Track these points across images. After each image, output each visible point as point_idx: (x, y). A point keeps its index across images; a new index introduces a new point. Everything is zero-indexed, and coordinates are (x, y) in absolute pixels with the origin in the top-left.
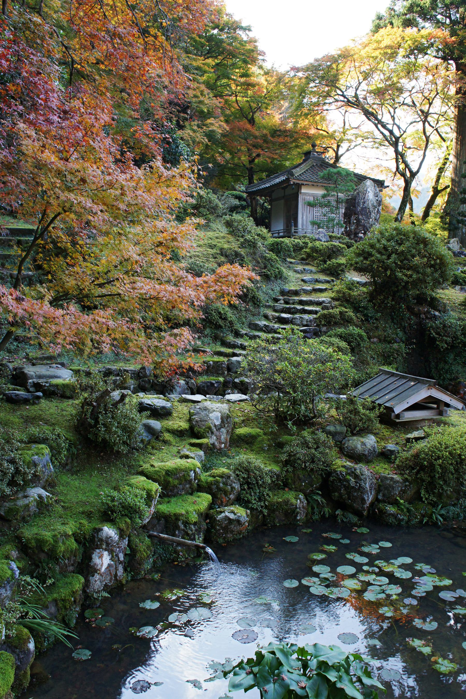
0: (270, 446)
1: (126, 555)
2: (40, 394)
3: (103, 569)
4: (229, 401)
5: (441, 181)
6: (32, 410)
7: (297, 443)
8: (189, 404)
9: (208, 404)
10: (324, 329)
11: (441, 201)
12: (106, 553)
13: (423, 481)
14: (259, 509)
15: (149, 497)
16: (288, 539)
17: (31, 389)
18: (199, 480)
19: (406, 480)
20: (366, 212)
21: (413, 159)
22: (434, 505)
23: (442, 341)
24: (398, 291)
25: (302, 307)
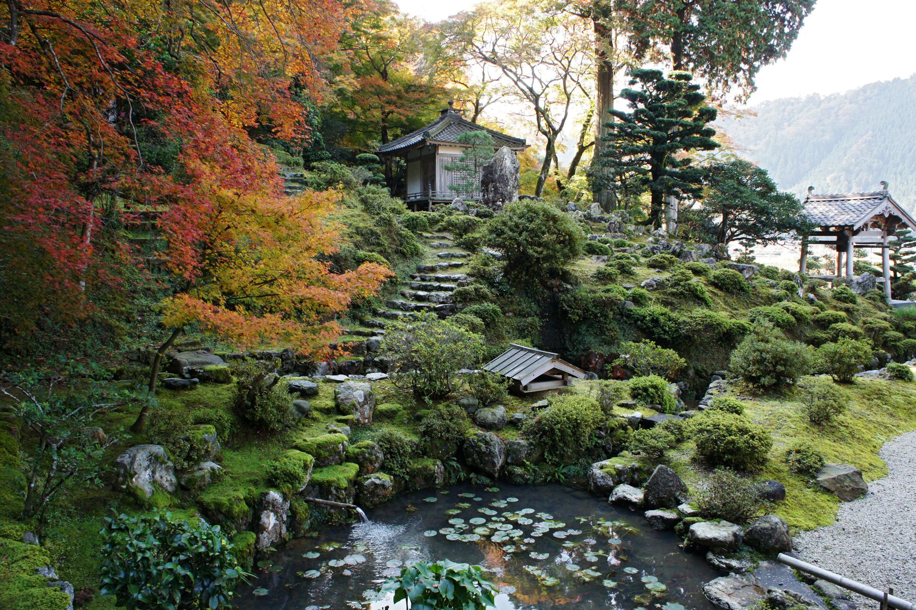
0: (409, 419)
1: (288, 516)
2: (196, 380)
3: (270, 528)
4: (370, 379)
5: (586, 137)
6: (192, 395)
8: (333, 384)
9: (351, 383)
10: (459, 305)
11: (588, 156)
12: (272, 514)
13: (546, 444)
14: (402, 475)
15: (306, 467)
16: (427, 500)
17: (187, 376)
18: (347, 452)
19: (531, 444)
20: (503, 180)
21: (556, 113)
22: (557, 465)
23: (573, 313)
24: (531, 266)
25: (438, 284)
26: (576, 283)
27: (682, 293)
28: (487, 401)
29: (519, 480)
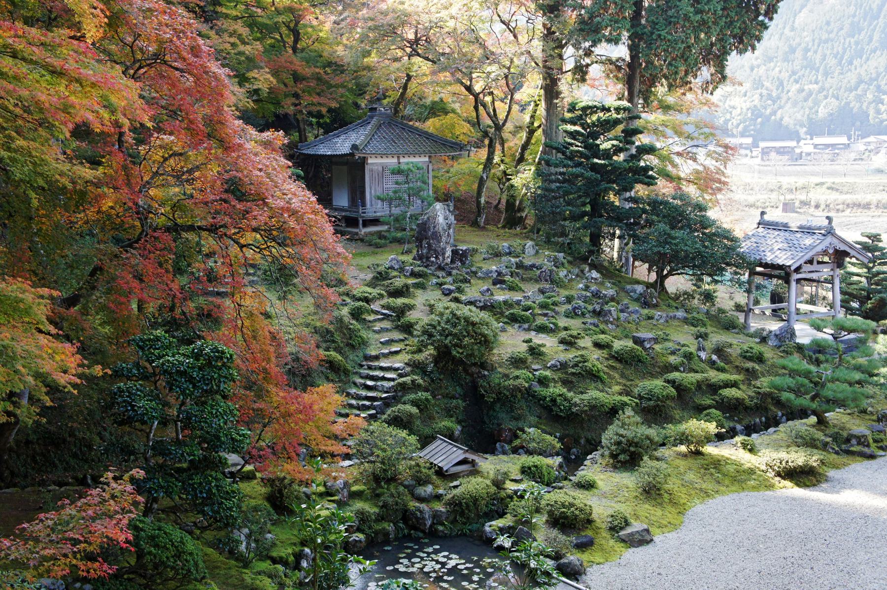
7: (389, 494)
20: (436, 236)
22: (465, 524)
23: (489, 397)
26: (493, 369)
27: (580, 373)
28: (421, 481)
29: (441, 534)
